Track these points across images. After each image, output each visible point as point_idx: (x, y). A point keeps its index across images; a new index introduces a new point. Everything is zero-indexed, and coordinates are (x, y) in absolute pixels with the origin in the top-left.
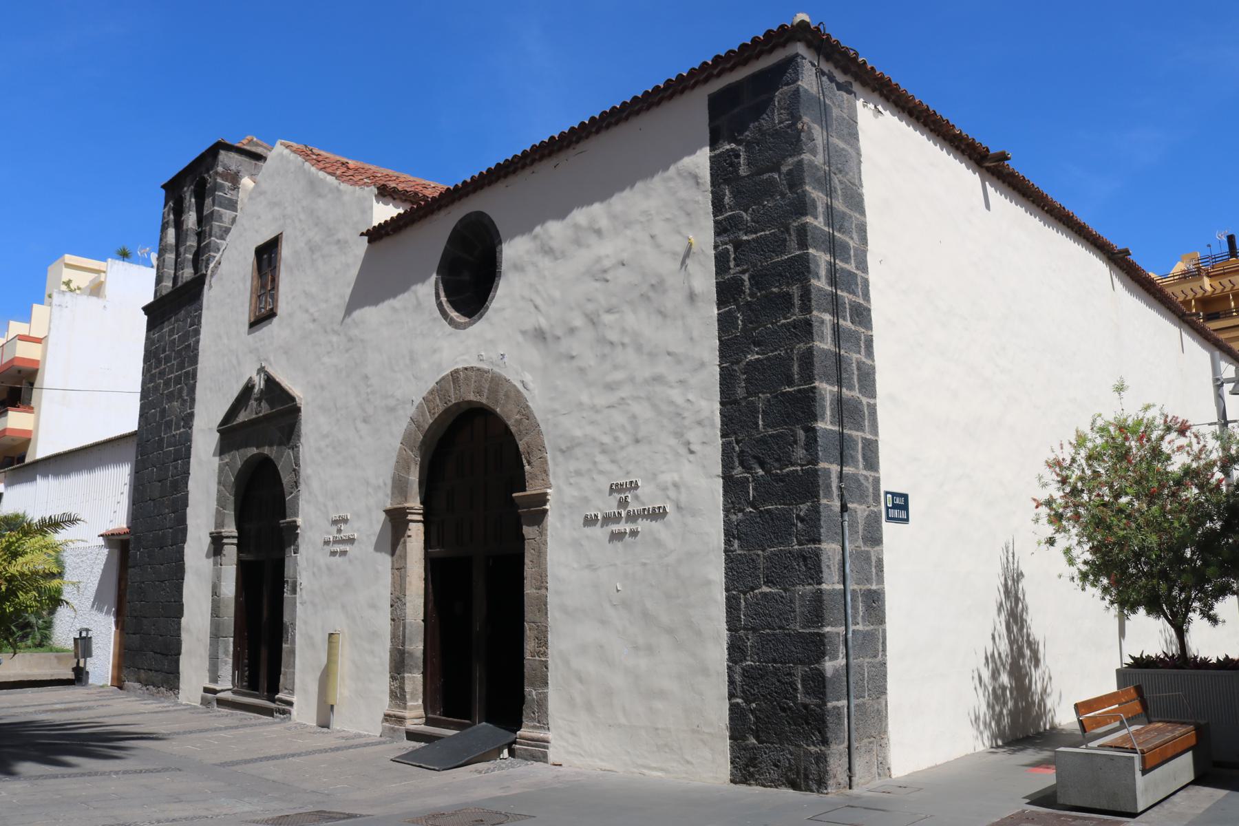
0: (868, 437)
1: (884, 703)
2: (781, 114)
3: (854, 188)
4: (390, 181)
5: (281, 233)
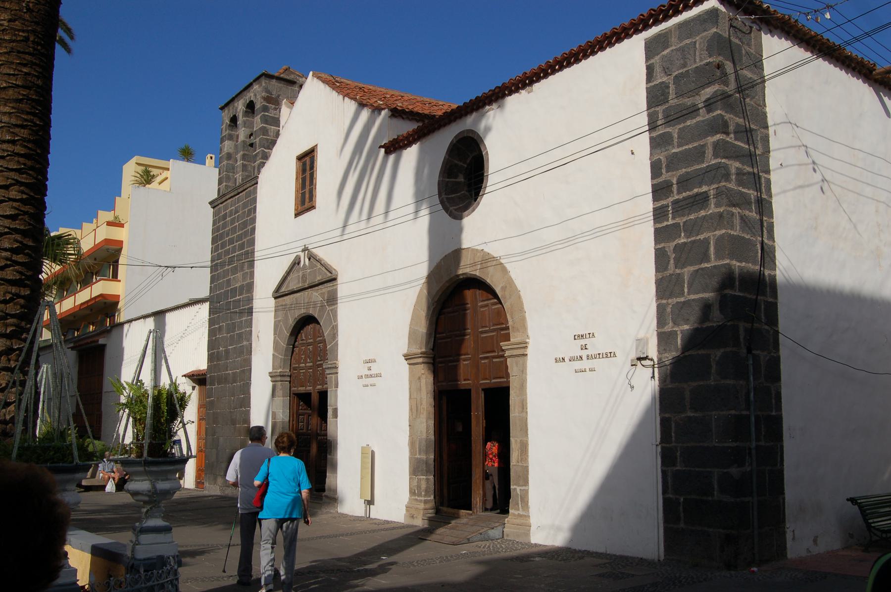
0: (769, 300)
1: (781, 501)
2: (702, 54)
3: (760, 108)
4: (396, 100)
5: (317, 145)
